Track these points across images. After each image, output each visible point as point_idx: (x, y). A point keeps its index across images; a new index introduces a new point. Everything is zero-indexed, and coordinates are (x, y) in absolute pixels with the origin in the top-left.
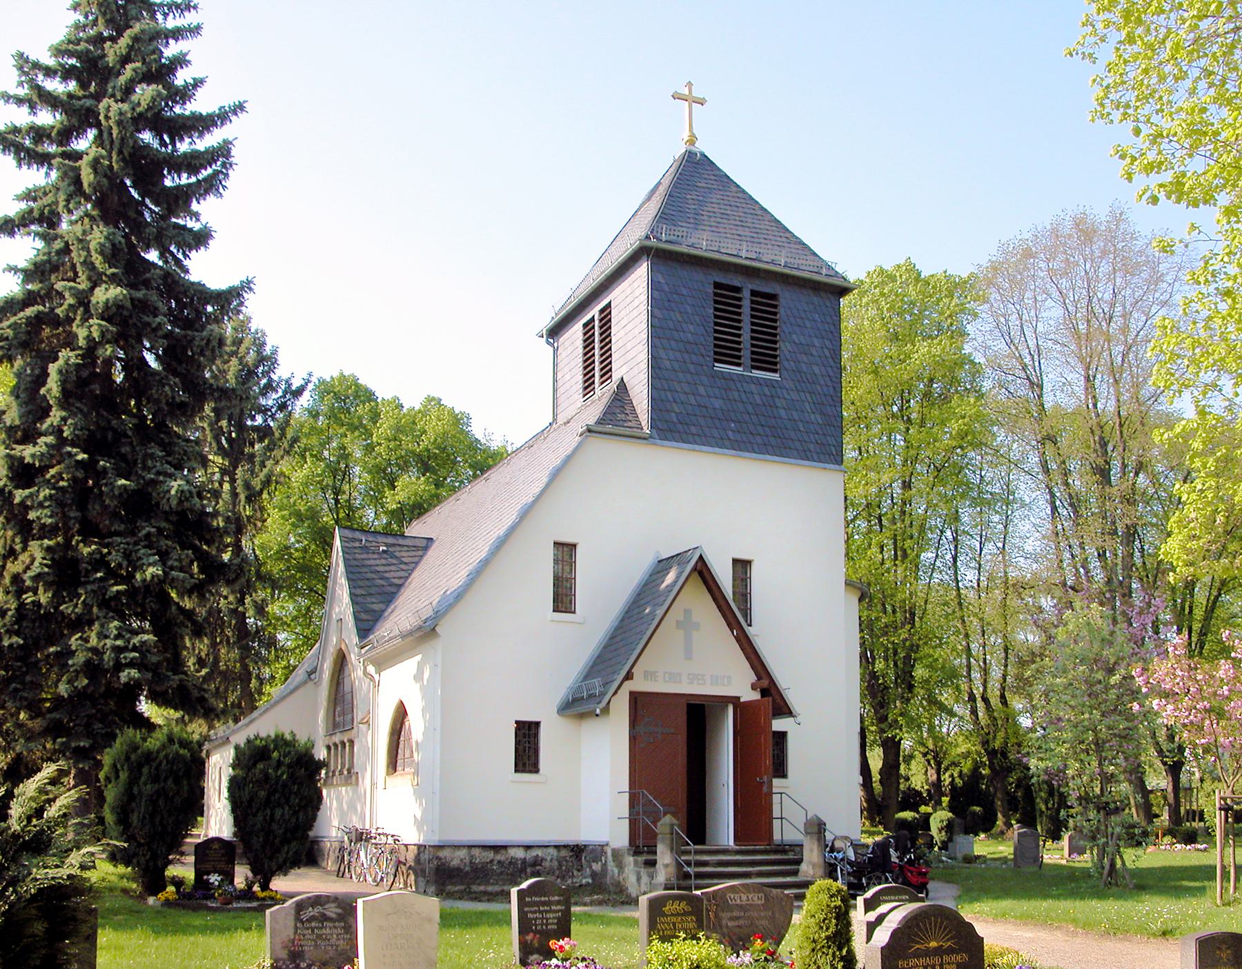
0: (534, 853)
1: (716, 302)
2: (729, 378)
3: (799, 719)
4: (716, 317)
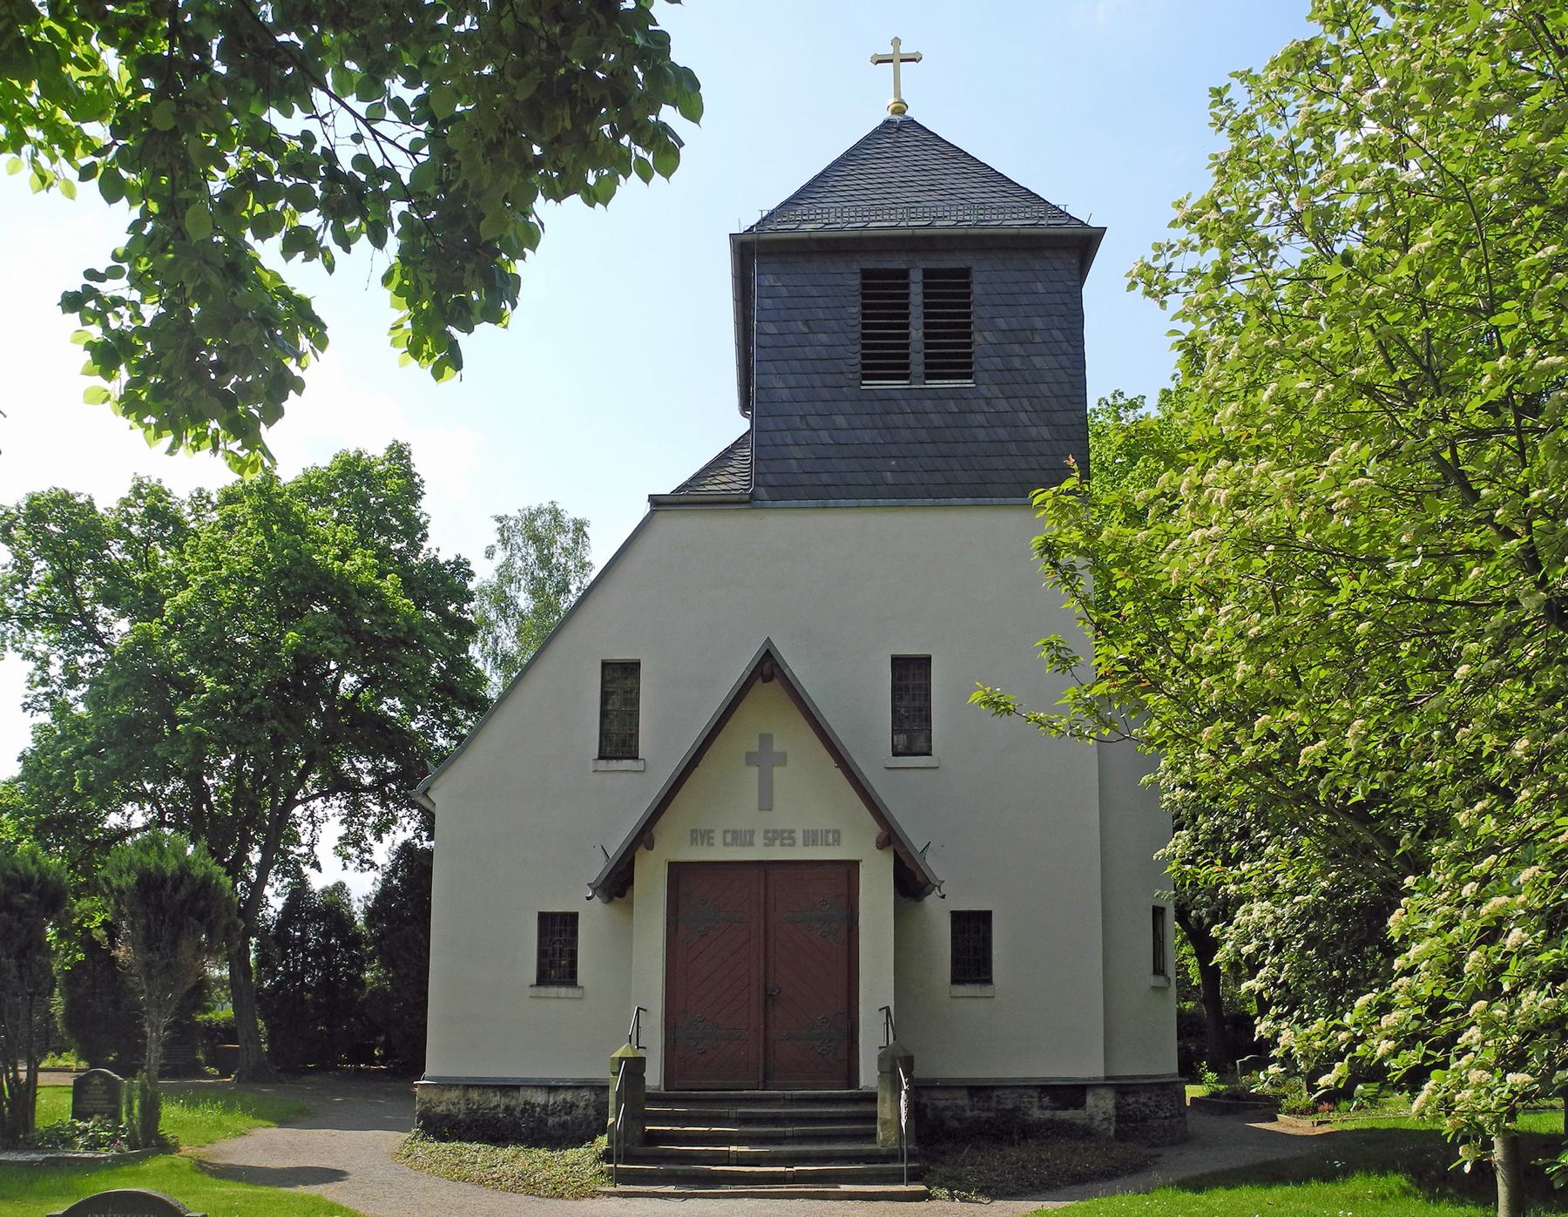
0: (561, 1096)
1: (865, 296)
2: (886, 398)
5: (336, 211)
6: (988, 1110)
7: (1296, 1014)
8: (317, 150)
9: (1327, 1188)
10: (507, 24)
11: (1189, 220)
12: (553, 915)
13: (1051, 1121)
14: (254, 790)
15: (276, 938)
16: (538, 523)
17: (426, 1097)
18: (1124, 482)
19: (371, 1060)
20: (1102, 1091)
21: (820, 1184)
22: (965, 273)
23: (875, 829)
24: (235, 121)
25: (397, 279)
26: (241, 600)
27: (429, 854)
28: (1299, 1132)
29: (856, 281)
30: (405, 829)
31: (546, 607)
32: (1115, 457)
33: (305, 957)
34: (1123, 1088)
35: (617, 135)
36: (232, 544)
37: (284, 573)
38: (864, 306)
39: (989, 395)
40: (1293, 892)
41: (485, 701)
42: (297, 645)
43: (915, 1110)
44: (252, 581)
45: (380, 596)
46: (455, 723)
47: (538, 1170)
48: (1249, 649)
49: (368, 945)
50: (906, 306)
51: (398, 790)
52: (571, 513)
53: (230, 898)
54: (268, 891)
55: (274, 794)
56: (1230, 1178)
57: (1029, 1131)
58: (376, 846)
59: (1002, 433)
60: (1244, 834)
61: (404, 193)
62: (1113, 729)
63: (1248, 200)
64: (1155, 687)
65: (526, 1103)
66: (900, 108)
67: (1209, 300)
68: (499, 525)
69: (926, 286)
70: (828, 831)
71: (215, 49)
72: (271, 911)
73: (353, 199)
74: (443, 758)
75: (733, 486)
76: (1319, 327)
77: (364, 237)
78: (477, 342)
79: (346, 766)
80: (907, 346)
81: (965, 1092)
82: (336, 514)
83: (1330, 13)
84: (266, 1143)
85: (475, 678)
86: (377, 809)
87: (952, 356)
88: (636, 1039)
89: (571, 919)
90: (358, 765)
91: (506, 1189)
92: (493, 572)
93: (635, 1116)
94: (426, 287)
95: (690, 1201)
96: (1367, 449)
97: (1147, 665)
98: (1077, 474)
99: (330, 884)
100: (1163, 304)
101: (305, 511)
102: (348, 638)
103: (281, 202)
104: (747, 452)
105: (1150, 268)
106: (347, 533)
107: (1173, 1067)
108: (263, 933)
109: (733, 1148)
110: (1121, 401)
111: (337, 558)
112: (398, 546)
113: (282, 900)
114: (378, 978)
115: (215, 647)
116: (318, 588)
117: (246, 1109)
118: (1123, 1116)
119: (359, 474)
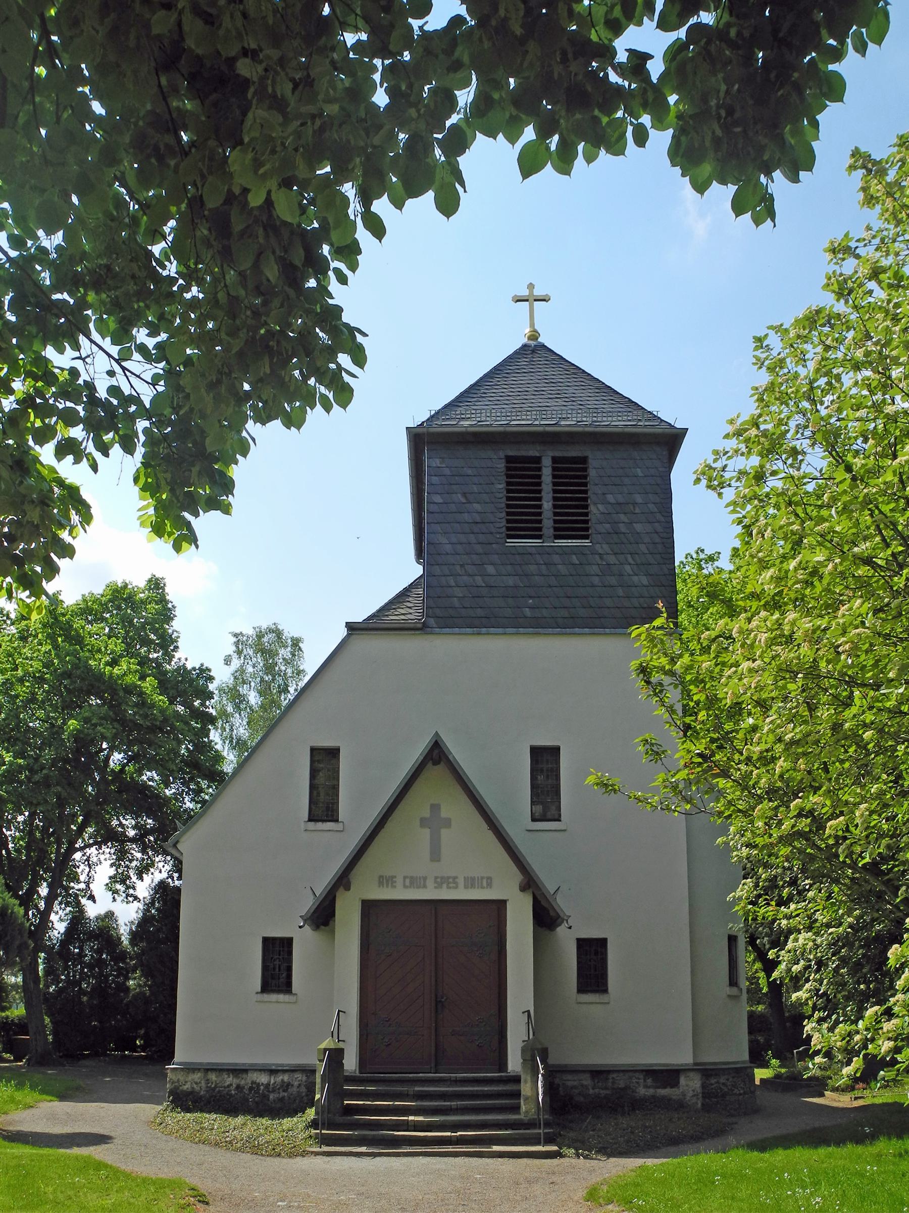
0: (280, 1078)
1: (508, 476)
5: (95, 427)
6: (606, 1088)
7: (834, 1017)
8: (81, 381)
9: (860, 1149)
10: (221, 296)
11: (738, 433)
12: (274, 939)
13: (653, 1097)
14: (43, 840)
15: (60, 953)
16: (265, 639)
17: (175, 1078)
18: (705, 616)
19: (134, 1048)
20: (691, 1074)
21: (477, 1146)
22: (584, 460)
23: (517, 877)
24: (22, 356)
25: (142, 480)
26: (34, 694)
27: (178, 890)
28: (840, 1105)
29: (501, 465)
30: (161, 871)
31: (269, 703)
32: (698, 598)
33: (82, 968)
34: (707, 1072)
35: (305, 378)
36: (26, 651)
37: (67, 675)
38: (508, 484)
39: (600, 551)
40: (828, 926)
41: (222, 774)
42: (77, 730)
43: (550, 1088)
44: (41, 680)
45: (141, 694)
46: (200, 791)
47: (261, 1135)
48: (786, 749)
49: (131, 959)
50: (539, 484)
51: (155, 842)
52: (290, 631)
53: (23, 923)
54: (53, 917)
55: (59, 843)
56: (786, 1141)
57: (637, 1105)
58: (139, 884)
59: (613, 580)
60: (793, 882)
61: (147, 414)
62: (692, 805)
63: (781, 420)
64: (725, 774)
65: (253, 1083)
66: (534, 335)
67: (752, 494)
68: (235, 639)
69: (554, 469)
70: (482, 878)
71: (6, 302)
72: (56, 932)
73: (108, 419)
74: (190, 818)
75: (409, 616)
76: (831, 516)
77: (117, 446)
78: (205, 523)
79: (115, 823)
80: (540, 514)
81: (588, 1075)
82: (107, 630)
83: (835, 287)
84: (47, 1114)
85: (215, 757)
86: (139, 855)
87: (573, 524)
88: (337, 1035)
89: (287, 943)
90: (124, 822)
91: (236, 1150)
92: (229, 675)
93: (337, 1093)
94: (163, 483)
95: (378, 1159)
96: (867, 605)
97: (717, 757)
98: (665, 615)
99: (103, 912)
100: (720, 495)
101: (83, 628)
102: (116, 725)
103: (54, 419)
104: (420, 591)
105: (710, 468)
106: (116, 646)
107: (746, 1056)
108: (49, 950)
109: (411, 1118)
110: (702, 556)
111: (107, 664)
112: (155, 655)
113: (65, 924)
114: (139, 985)
115: (12, 730)
116: (92, 686)
117: (33, 1088)
118: (706, 1093)
119: (125, 600)
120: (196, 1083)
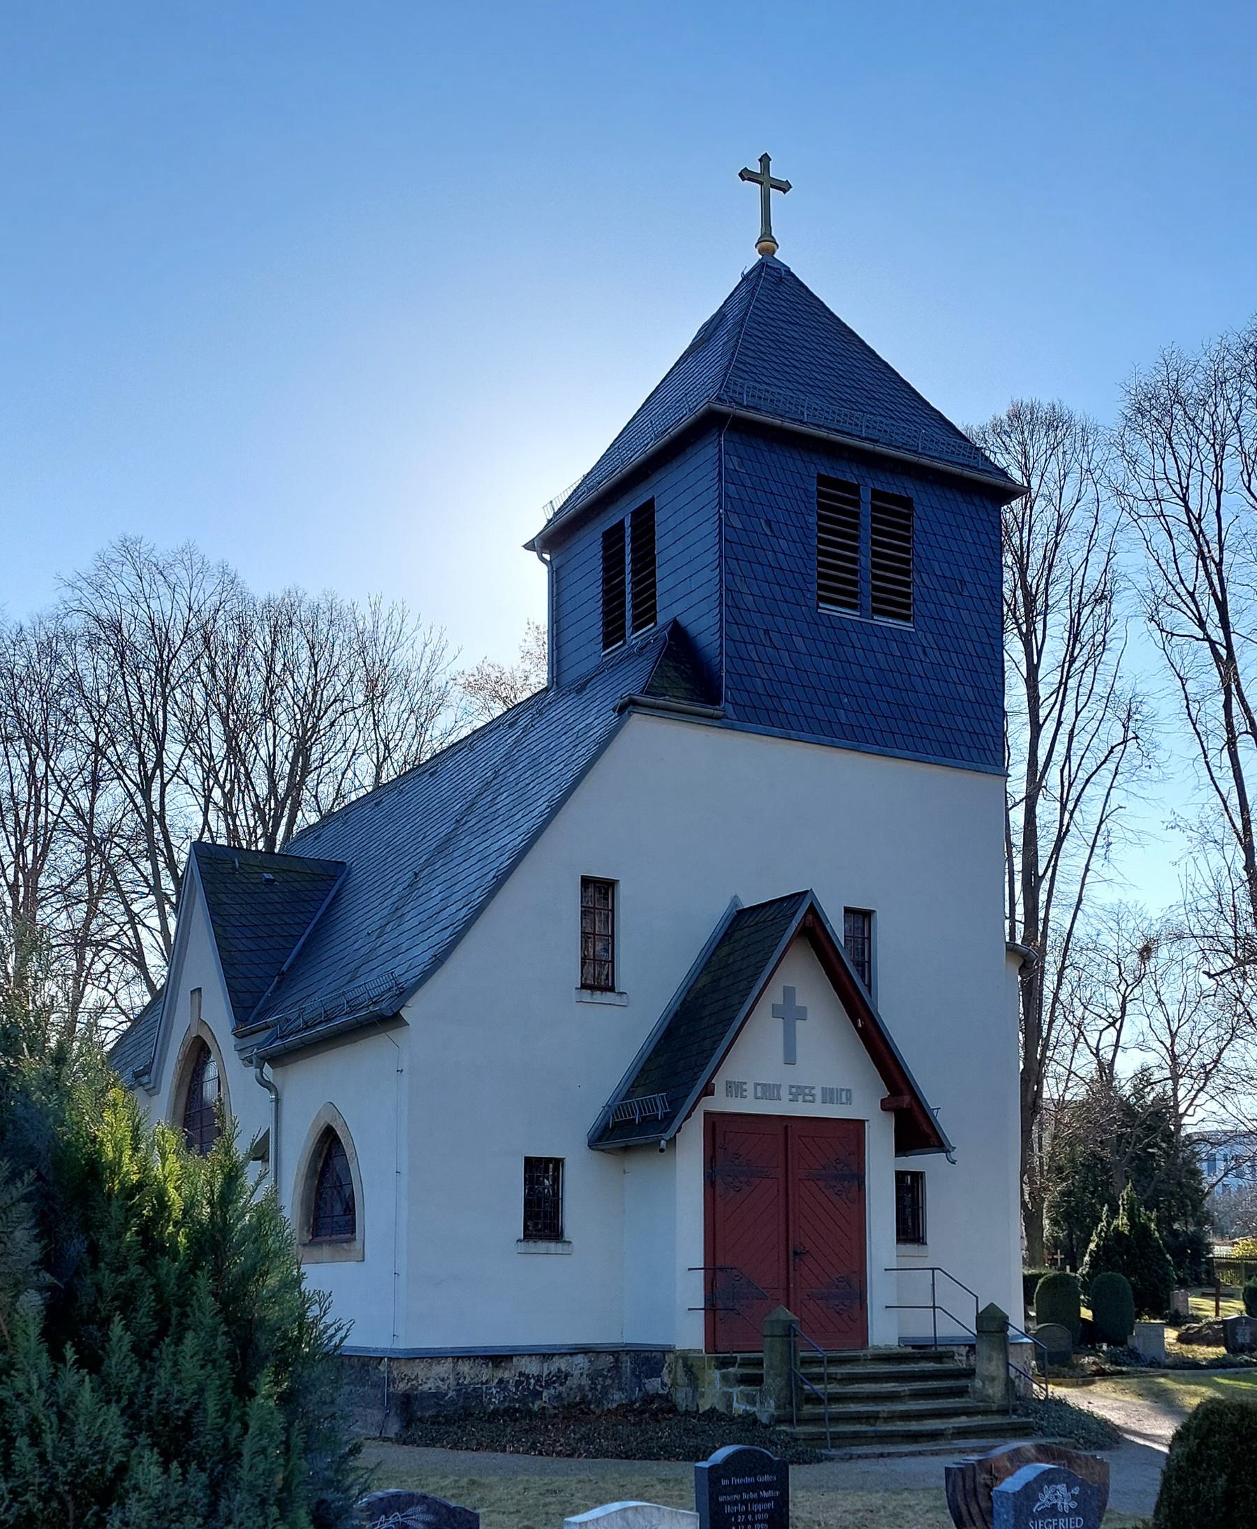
2: (837, 626)
3: (953, 1155)
4: (821, 529)
65: (521, 1374)
120: (443, 1380)
